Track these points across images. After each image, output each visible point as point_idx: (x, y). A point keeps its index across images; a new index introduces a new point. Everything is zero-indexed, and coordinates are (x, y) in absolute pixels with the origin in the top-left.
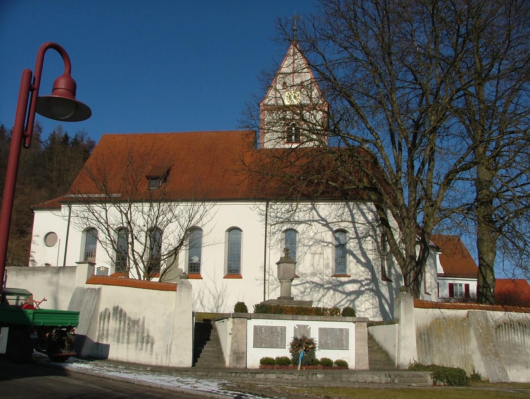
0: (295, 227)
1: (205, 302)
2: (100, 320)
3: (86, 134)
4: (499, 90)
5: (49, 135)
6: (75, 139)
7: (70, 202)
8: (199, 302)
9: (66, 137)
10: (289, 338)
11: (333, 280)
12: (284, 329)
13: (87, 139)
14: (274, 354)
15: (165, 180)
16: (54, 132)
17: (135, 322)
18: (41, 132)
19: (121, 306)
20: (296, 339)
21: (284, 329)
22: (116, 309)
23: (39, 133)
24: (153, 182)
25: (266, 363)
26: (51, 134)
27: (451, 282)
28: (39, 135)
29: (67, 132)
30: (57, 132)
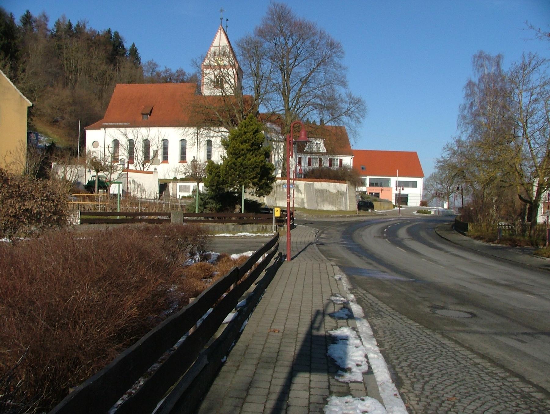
0: (211, 139)
1: (170, 174)
2: (387, 221)
3: (88, 22)
4: (309, 72)
5: (54, 23)
6: (78, 26)
7: (105, 127)
8: (167, 174)
9: (70, 25)
10: (191, 190)
11: (319, 140)
12: (190, 186)
13: (90, 28)
14: (186, 194)
15: (150, 115)
16: (59, 20)
17: (139, 185)
18: (47, 21)
19: (134, 179)
20: (193, 189)
21: (190, 186)
22: (133, 180)
23: (46, 22)
24: (145, 116)
25: (184, 197)
26: (56, 22)
27: (330, 157)
28: (46, 25)
29: (70, 20)
30: (61, 21)
